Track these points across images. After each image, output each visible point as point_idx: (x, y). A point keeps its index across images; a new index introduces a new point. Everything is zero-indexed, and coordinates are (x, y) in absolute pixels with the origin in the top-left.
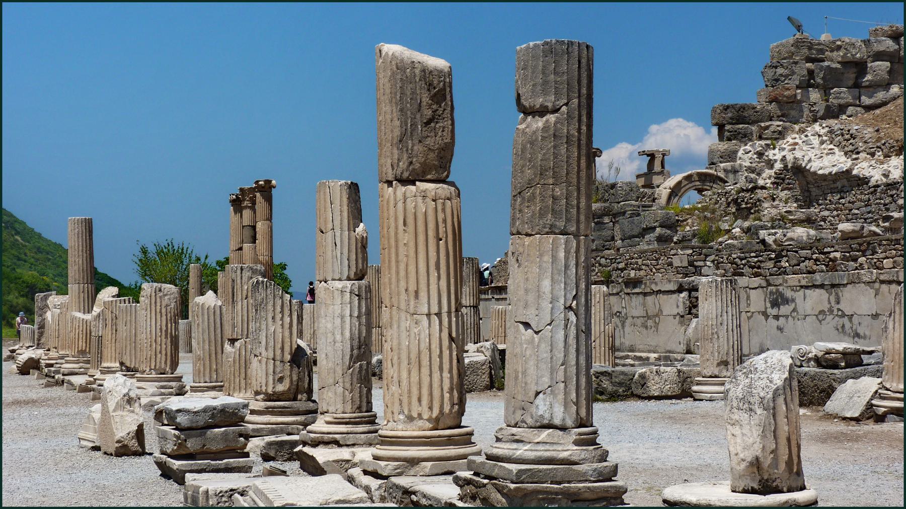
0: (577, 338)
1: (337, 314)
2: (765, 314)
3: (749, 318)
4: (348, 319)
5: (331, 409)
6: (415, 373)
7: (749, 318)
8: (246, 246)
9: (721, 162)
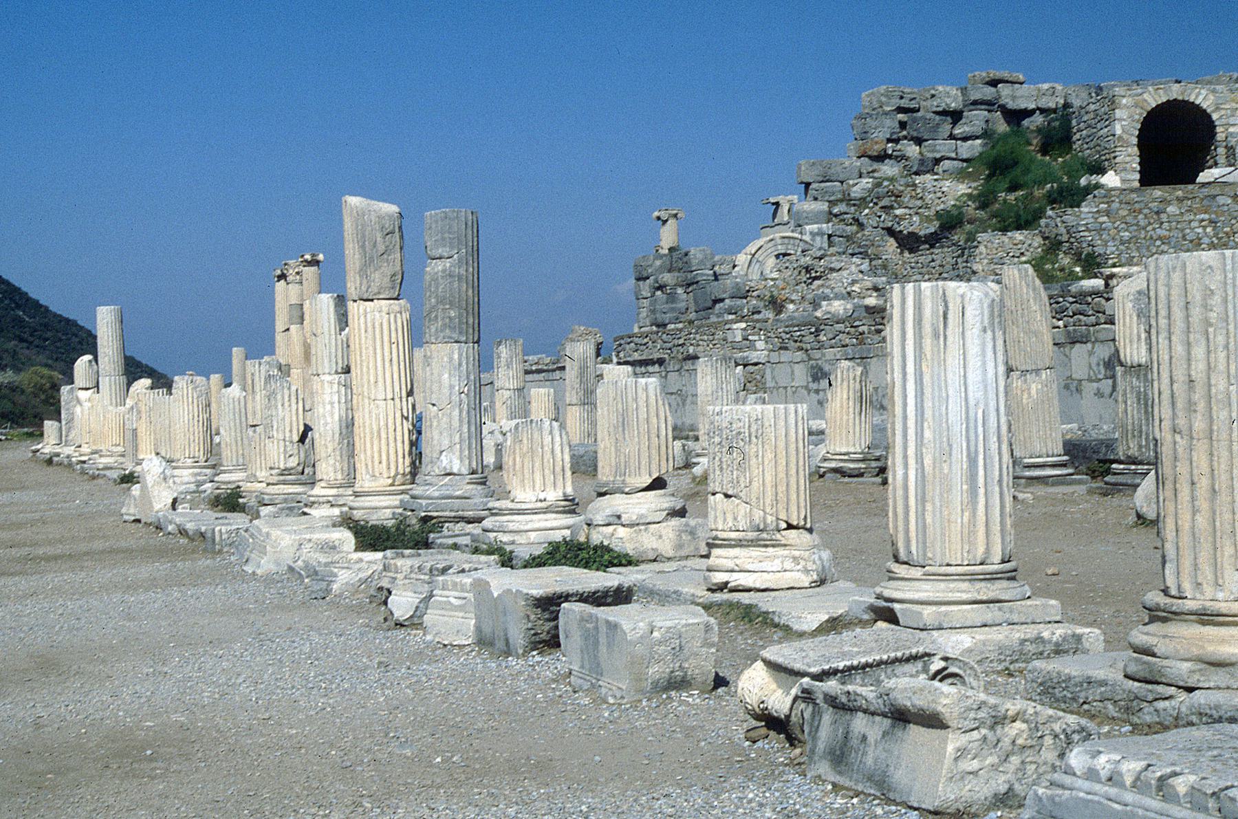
0: (468, 412)
1: (327, 401)
2: (806, 388)
3: (794, 393)
4: (336, 405)
5: (325, 477)
6: (376, 442)
7: (794, 393)
8: (293, 328)
9: (807, 224)
